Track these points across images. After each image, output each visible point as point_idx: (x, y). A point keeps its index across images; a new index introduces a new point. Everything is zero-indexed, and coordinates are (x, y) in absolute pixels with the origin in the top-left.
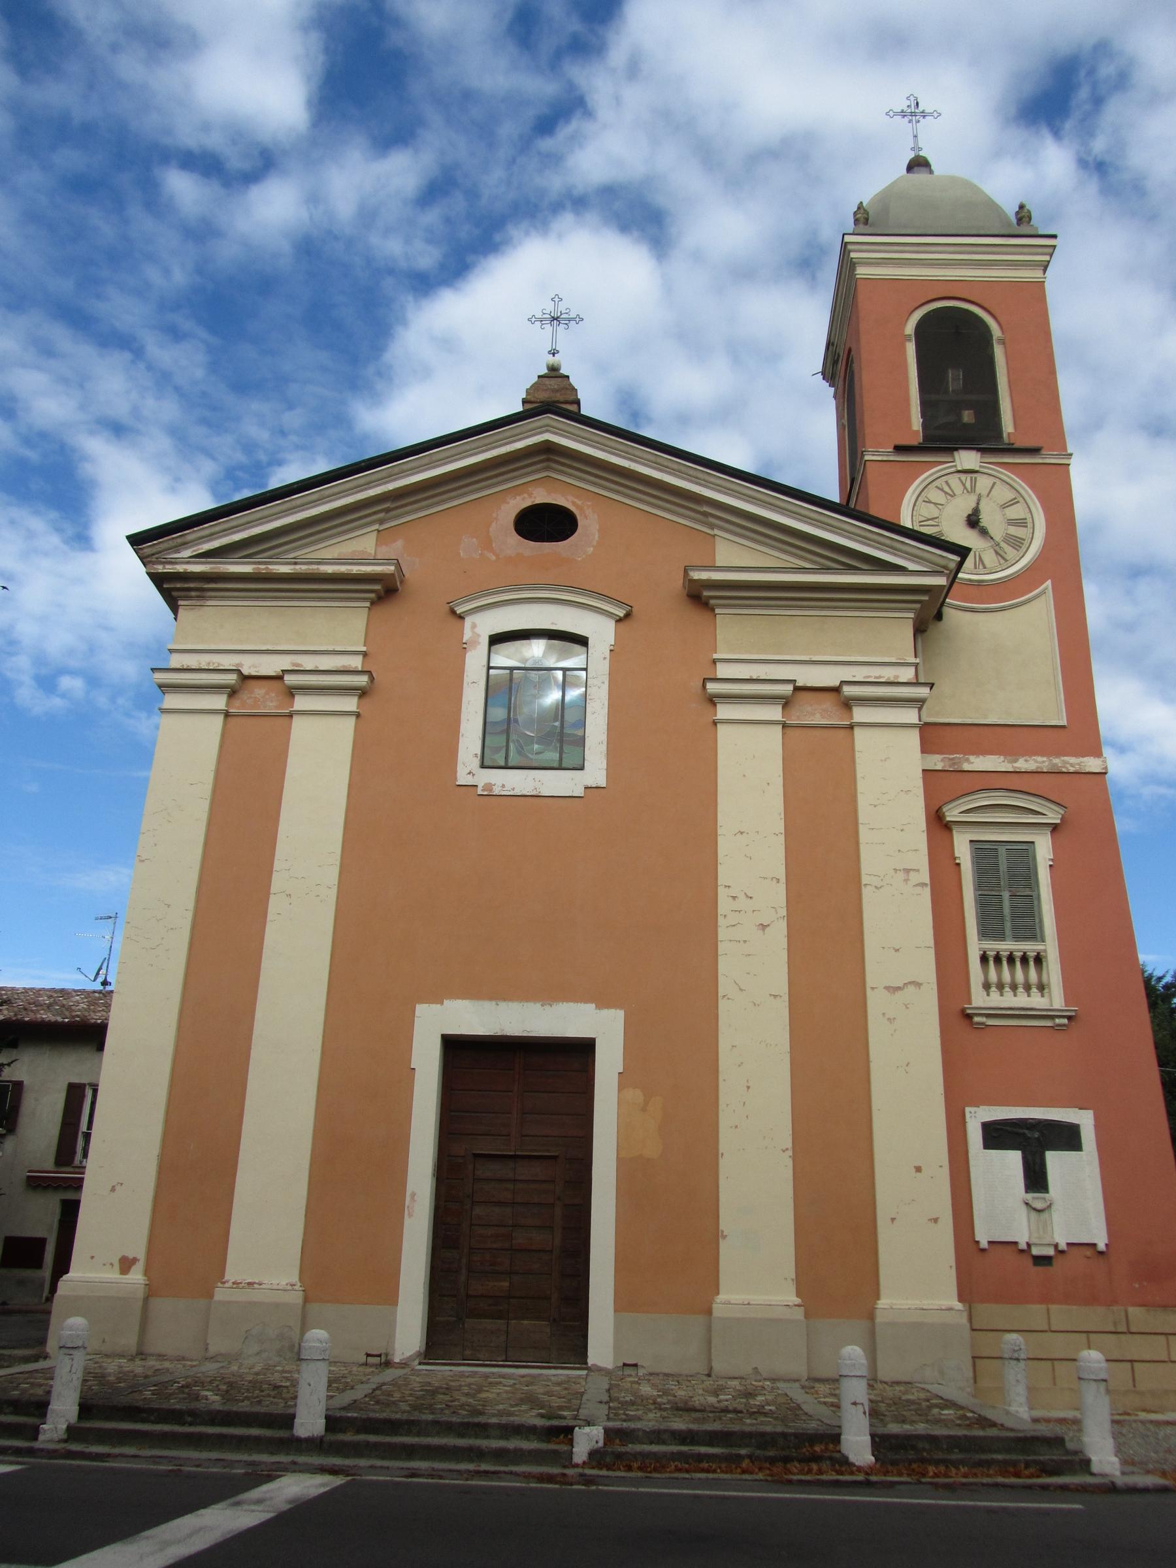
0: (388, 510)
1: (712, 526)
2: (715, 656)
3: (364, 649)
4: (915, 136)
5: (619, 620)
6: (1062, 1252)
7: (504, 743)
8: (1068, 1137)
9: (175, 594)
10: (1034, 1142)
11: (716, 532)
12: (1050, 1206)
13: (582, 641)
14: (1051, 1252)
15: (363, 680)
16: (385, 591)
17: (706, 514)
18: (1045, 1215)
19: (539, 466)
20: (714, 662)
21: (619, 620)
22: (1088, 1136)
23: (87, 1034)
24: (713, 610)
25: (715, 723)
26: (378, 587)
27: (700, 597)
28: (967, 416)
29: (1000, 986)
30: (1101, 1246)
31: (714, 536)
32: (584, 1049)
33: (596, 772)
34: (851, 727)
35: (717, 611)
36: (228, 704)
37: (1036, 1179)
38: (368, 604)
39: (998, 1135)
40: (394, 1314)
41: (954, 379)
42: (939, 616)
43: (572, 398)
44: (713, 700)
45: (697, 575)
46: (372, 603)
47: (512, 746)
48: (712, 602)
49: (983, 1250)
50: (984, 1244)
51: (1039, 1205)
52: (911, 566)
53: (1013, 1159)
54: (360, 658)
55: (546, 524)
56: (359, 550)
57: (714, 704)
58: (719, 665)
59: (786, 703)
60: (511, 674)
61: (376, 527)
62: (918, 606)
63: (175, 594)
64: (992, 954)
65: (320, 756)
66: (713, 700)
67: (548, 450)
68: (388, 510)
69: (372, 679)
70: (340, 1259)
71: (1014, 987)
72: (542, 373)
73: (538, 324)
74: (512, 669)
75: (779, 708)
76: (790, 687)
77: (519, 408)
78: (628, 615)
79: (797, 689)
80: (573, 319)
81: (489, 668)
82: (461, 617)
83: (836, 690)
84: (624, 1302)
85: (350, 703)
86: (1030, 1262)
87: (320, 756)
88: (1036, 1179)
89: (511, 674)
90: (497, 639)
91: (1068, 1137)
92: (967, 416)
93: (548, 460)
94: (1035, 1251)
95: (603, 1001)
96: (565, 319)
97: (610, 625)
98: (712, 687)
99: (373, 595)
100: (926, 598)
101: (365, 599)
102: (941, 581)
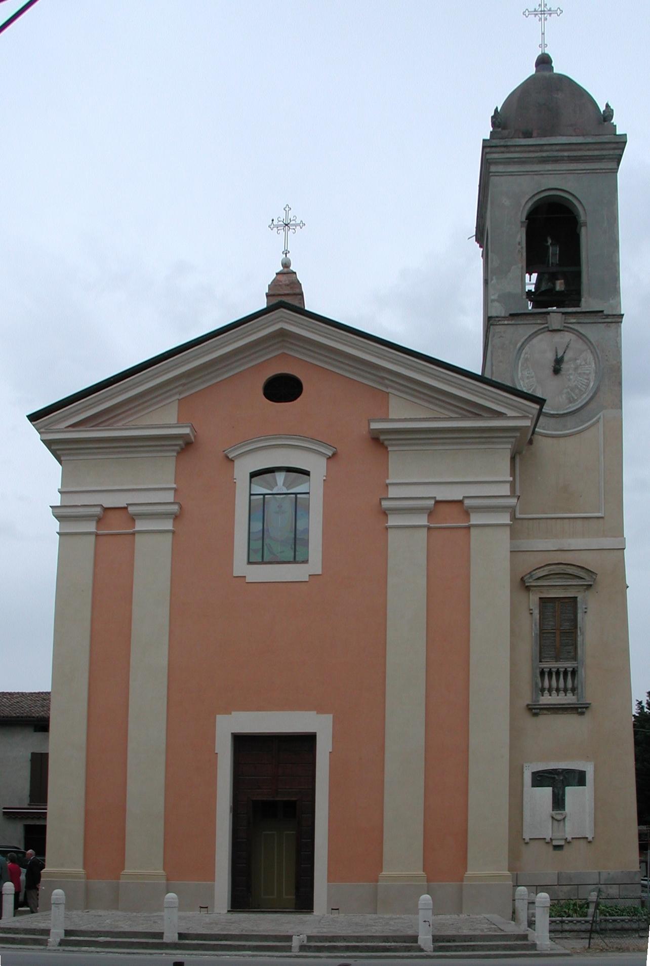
0: (184, 385)
1: (387, 386)
2: (388, 481)
3: (174, 486)
4: (543, 34)
5: (329, 458)
6: (569, 843)
7: (260, 554)
8: (579, 778)
9: (58, 452)
10: (558, 781)
11: (389, 390)
12: (564, 819)
13: (307, 473)
14: (562, 843)
15: (175, 508)
16: (186, 445)
17: (383, 378)
18: (562, 823)
19: (275, 347)
20: (387, 485)
21: (329, 458)
22: (589, 778)
23: (42, 725)
24: (387, 448)
25: (387, 528)
26: (181, 442)
27: (378, 440)
28: (560, 285)
29: (550, 690)
30: (590, 839)
31: (388, 393)
32: (309, 740)
33: (315, 564)
34: (468, 528)
35: (390, 449)
36: (97, 528)
37: (558, 802)
38: (175, 454)
39: (540, 779)
40: (618, 335)
41: (553, 252)
42: (531, 442)
43: (298, 291)
44: (385, 513)
45: (375, 426)
46: (178, 453)
47: (265, 547)
48: (386, 443)
49: (527, 843)
50: (527, 840)
51: (559, 817)
52: (510, 413)
53: (547, 792)
54: (172, 493)
55: (283, 389)
56: (165, 419)
57: (387, 515)
58: (390, 488)
59: (431, 513)
60: (264, 498)
61: (177, 397)
62: (513, 440)
63: (58, 452)
64: (546, 670)
65: (153, 560)
66: (385, 513)
67: (282, 334)
68: (184, 385)
69: (181, 508)
70: (183, 863)
71: (558, 690)
72: (278, 271)
73: (275, 229)
74: (264, 495)
75: (425, 517)
76: (433, 502)
77: (263, 305)
78: (334, 454)
79: (438, 502)
80: (299, 225)
81: (251, 495)
82: (232, 461)
83: (460, 502)
84: (332, 876)
85: (168, 525)
86: (551, 848)
87: (153, 560)
88: (558, 802)
89: (264, 498)
90: (253, 475)
91: (579, 778)
92: (560, 285)
93: (283, 341)
94: (555, 843)
95: (320, 709)
96: (293, 225)
97: (323, 462)
98: (385, 504)
99: (177, 448)
100: (518, 434)
101: (173, 450)
102: (527, 423)
